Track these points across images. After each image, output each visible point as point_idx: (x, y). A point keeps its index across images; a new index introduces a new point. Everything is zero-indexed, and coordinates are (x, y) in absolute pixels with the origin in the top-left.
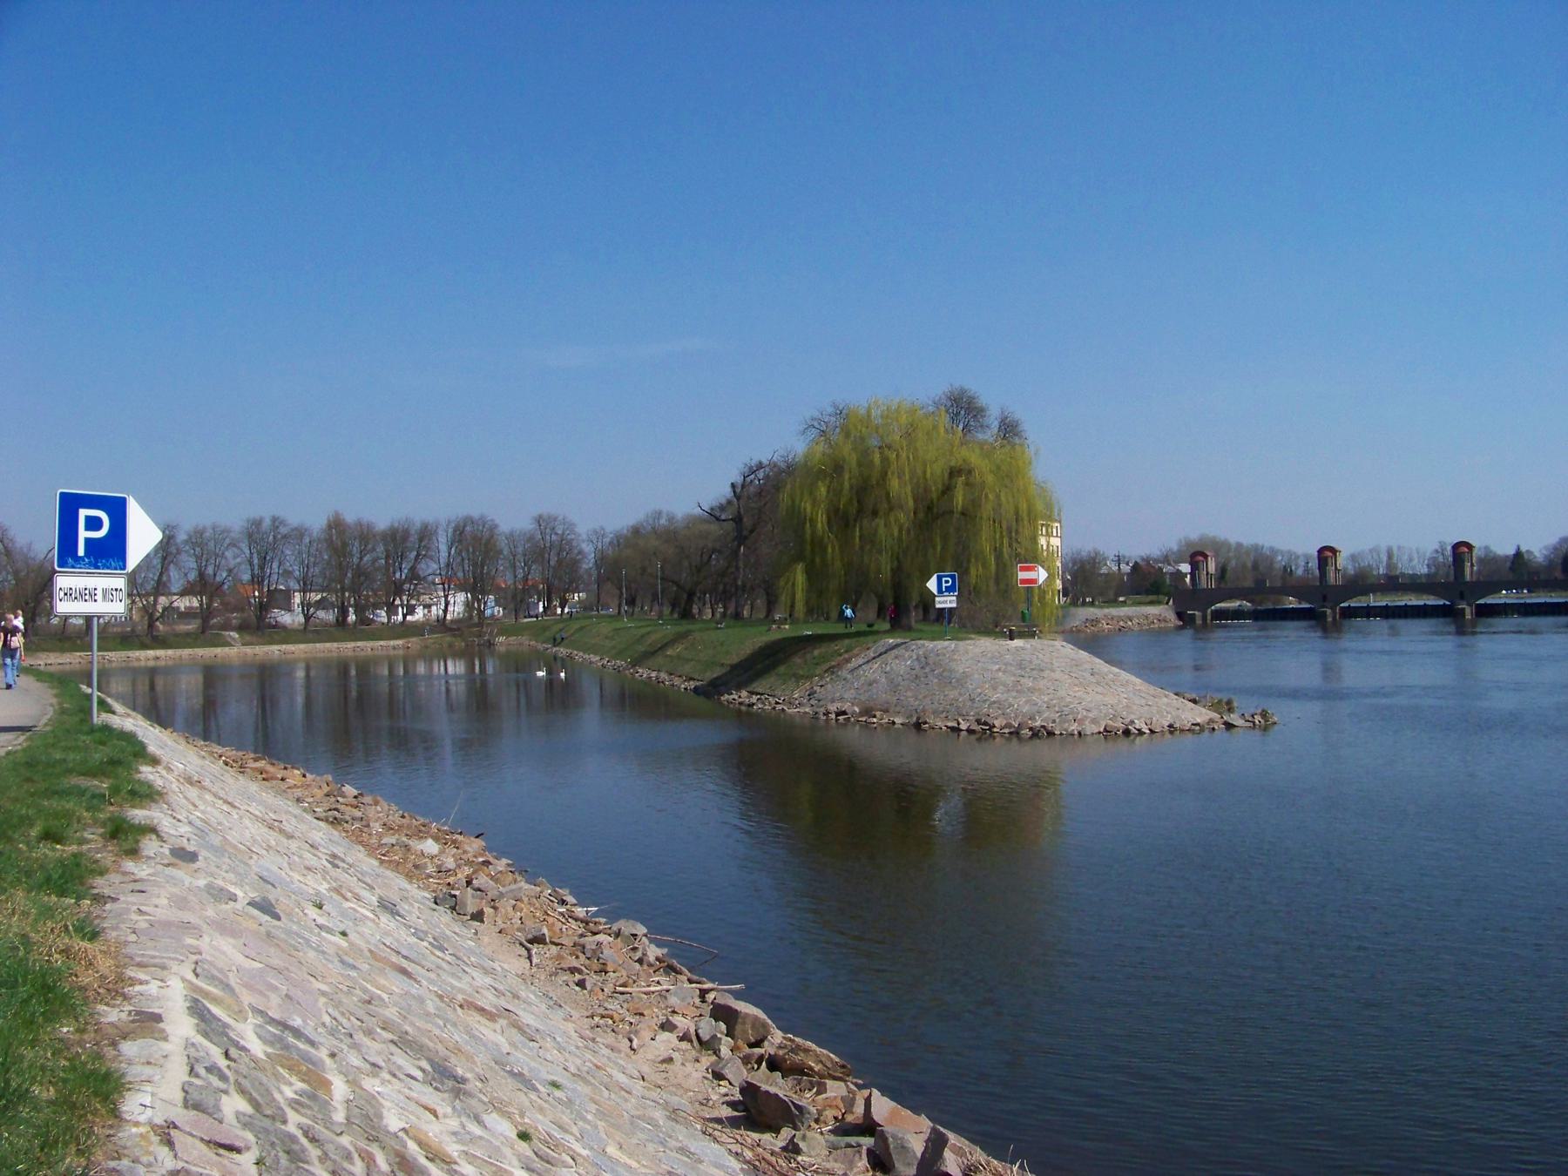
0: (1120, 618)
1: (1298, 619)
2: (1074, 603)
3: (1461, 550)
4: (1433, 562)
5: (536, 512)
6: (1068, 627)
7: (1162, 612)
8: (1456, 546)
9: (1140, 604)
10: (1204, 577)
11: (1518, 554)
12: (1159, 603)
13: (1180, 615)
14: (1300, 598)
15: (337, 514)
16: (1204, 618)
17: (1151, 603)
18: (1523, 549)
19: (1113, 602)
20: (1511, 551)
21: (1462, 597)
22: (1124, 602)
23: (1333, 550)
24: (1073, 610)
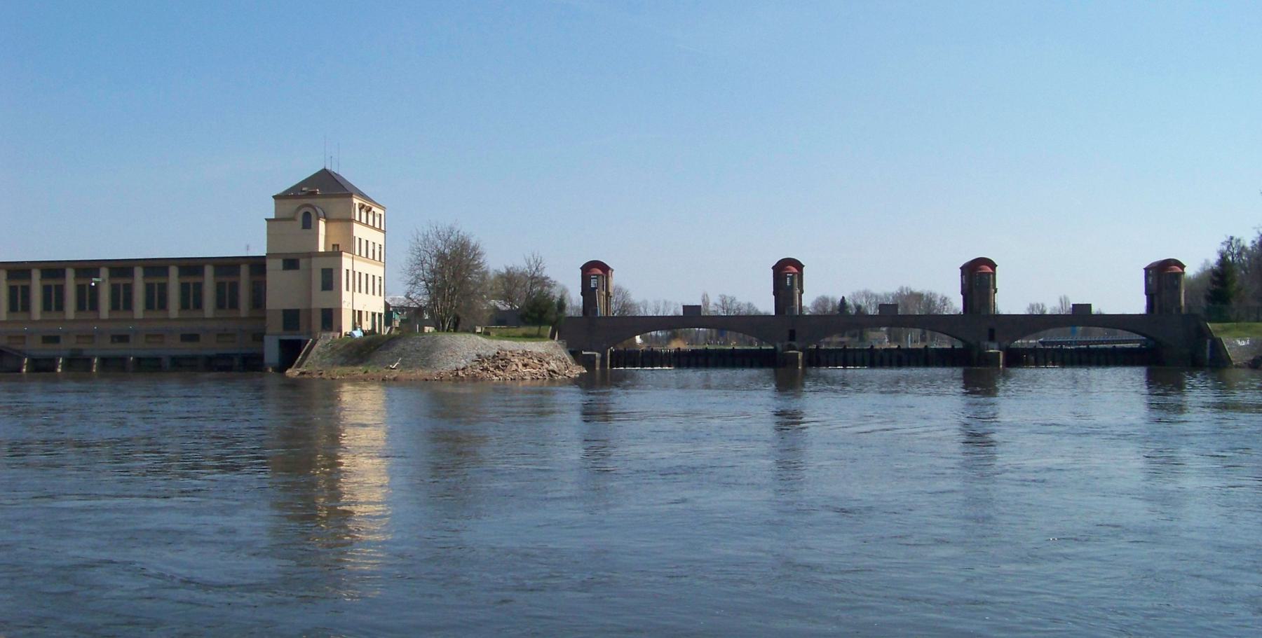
7: (548, 352)
12: (539, 337)
13: (575, 354)
16: (603, 359)
21: (992, 338)
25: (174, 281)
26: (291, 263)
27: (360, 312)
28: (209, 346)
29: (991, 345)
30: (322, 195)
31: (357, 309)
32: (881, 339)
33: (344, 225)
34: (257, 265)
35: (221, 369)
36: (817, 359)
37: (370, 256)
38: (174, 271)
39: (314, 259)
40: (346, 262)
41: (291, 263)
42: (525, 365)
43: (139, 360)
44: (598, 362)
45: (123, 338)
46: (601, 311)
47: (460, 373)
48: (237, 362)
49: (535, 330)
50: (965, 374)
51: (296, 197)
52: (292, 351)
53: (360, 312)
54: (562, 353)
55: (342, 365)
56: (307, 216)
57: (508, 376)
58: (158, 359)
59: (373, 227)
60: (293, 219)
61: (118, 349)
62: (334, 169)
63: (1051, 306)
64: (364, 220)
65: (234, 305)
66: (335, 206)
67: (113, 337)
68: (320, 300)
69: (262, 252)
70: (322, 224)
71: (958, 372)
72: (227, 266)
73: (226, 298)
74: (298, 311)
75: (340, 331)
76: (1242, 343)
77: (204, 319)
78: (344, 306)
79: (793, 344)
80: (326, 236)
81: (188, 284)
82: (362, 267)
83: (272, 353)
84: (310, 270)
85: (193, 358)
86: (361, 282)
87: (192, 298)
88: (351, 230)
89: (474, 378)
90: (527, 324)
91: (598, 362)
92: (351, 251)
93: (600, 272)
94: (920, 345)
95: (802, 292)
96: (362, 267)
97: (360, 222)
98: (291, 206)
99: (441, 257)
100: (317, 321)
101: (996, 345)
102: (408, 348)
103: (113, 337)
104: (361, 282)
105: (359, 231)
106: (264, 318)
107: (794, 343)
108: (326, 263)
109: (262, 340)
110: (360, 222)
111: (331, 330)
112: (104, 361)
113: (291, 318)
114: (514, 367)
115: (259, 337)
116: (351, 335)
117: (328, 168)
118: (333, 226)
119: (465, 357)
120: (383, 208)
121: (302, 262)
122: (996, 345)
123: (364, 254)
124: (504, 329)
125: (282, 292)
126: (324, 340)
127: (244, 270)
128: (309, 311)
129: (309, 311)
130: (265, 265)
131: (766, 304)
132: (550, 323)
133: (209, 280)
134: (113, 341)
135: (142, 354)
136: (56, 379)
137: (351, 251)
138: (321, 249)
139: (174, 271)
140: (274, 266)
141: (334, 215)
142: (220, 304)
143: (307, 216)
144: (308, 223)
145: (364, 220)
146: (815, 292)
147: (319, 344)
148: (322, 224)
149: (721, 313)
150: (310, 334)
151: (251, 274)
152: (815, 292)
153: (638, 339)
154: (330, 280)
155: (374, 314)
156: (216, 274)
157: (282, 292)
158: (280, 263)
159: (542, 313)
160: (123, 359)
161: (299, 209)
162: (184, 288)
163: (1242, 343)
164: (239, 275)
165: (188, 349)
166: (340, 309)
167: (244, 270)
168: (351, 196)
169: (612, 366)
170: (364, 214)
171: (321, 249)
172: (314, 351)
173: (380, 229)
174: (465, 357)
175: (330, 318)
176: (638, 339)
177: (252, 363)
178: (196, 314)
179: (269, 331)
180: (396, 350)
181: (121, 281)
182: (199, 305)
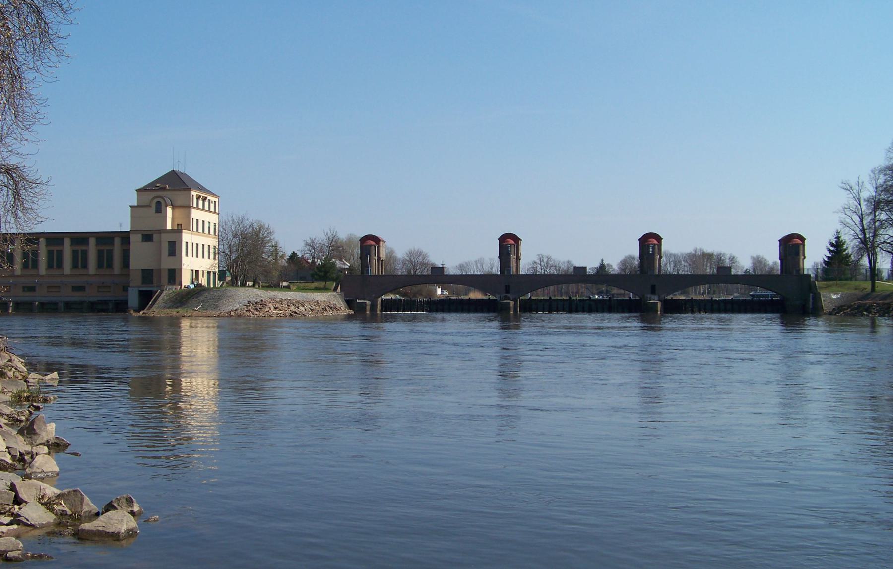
0: (290, 303)
1: (476, 311)
2: (233, 283)
3: (370, 243)
4: (625, 263)
5: (735, 254)
6: (224, 310)
7: (330, 298)
8: (364, 239)
9: (304, 289)
10: (375, 262)
11: (602, 267)
12: (325, 289)
13: (349, 303)
14: (484, 291)
15: (753, 258)
16: (373, 307)
17: (317, 289)
18: (605, 263)
19: (276, 286)
20: (597, 265)
21: (653, 291)
22: (288, 287)
23: (376, 240)
24: (232, 290)
25: (67, 248)
26: (148, 237)
27: (197, 272)
28: (92, 295)
29: (653, 297)
30: (171, 188)
31: (194, 269)
32: (699, 293)
33: (186, 210)
34: (125, 237)
35: (99, 311)
36: (529, 307)
37: (206, 231)
38: (67, 242)
39: (163, 235)
40: (186, 236)
41: (148, 237)
42: (276, 308)
43: (42, 304)
44: (368, 307)
45: (32, 289)
46: (374, 271)
47: (232, 313)
48: (111, 306)
49: (322, 284)
50: (641, 316)
51: (152, 190)
52: (146, 298)
53: (197, 272)
54: (340, 303)
55: (169, 308)
56: (159, 203)
57: (261, 314)
58: (56, 303)
59: (209, 211)
60: (149, 206)
61: (27, 297)
62: (180, 169)
63: (591, 265)
64: (201, 206)
65: (110, 266)
66: (179, 198)
67: (24, 287)
68: (167, 263)
69: (127, 227)
70: (169, 210)
71: (778, 315)
72: (105, 238)
73: (105, 260)
74: (152, 270)
75: (181, 285)
76: (834, 296)
77: (89, 275)
78: (183, 267)
79: (511, 294)
80: (173, 218)
81: (103, 250)
82: (198, 239)
83: (133, 298)
84: (160, 242)
85: (82, 303)
86: (197, 250)
87: (80, 261)
88: (190, 214)
89: (239, 316)
90: (316, 280)
91: (368, 307)
92: (189, 228)
93: (373, 243)
94: (706, 297)
95: (518, 259)
96: (198, 239)
97: (197, 208)
98: (149, 196)
99: (258, 233)
100: (165, 277)
101: (656, 297)
102: (209, 297)
103: (24, 287)
104: (197, 250)
105: (196, 214)
106: (129, 275)
107: (509, 295)
108: (171, 237)
109: (127, 290)
110: (197, 208)
111: (174, 284)
112: (17, 305)
113: (148, 275)
114: (267, 309)
115: (125, 289)
116: (188, 287)
117: (176, 169)
118: (177, 211)
119: (239, 303)
120: (218, 197)
121: (155, 236)
122: (656, 297)
123: (200, 230)
124: (303, 284)
125: (141, 257)
126: (169, 291)
127: (117, 241)
128: (160, 271)
129: (159, 271)
130: (129, 238)
131: (496, 270)
132: (333, 280)
133: (92, 248)
134: (24, 291)
135: (44, 300)
136: (9, 314)
137: (189, 228)
138: (169, 227)
139: (67, 242)
140: (135, 239)
141: (179, 203)
142: (100, 265)
143: (159, 203)
144: (160, 209)
145: (201, 206)
146: (528, 260)
147: (164, 293)
148: (169, 210)
149: (459, 273)
150: (159, 286)
151: (122, 244)
152: (528, 260)
153: (439, 291)
154: (174, 249)
155: (209, 273)
156: (97, 244)
157: (141, 257)
158: (140, 236)
159: (326, 272)
160: (31, 303)
161: (154, 198)
162: (75, 253)
163: (834, 296)
164: (88, 244)
165: (77, 297)
166: (181, 269)
167: (117, 241)
168: (190, 190)
169: (382, 310)
170: (201, 202)
171: (169, 227)
172: (160, 298)
173: (215, 212)
174: (239, 303)
175: (174, 275)
176: (439, 291)
177: (121, 307)
178: (33, 272)
179: (131, 284)
180: (202, 298)
181: (55, 248)
182: (85, 266)
